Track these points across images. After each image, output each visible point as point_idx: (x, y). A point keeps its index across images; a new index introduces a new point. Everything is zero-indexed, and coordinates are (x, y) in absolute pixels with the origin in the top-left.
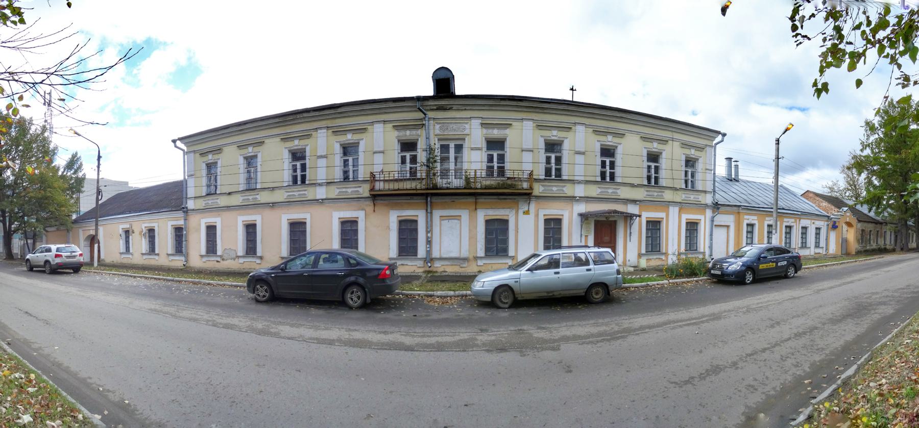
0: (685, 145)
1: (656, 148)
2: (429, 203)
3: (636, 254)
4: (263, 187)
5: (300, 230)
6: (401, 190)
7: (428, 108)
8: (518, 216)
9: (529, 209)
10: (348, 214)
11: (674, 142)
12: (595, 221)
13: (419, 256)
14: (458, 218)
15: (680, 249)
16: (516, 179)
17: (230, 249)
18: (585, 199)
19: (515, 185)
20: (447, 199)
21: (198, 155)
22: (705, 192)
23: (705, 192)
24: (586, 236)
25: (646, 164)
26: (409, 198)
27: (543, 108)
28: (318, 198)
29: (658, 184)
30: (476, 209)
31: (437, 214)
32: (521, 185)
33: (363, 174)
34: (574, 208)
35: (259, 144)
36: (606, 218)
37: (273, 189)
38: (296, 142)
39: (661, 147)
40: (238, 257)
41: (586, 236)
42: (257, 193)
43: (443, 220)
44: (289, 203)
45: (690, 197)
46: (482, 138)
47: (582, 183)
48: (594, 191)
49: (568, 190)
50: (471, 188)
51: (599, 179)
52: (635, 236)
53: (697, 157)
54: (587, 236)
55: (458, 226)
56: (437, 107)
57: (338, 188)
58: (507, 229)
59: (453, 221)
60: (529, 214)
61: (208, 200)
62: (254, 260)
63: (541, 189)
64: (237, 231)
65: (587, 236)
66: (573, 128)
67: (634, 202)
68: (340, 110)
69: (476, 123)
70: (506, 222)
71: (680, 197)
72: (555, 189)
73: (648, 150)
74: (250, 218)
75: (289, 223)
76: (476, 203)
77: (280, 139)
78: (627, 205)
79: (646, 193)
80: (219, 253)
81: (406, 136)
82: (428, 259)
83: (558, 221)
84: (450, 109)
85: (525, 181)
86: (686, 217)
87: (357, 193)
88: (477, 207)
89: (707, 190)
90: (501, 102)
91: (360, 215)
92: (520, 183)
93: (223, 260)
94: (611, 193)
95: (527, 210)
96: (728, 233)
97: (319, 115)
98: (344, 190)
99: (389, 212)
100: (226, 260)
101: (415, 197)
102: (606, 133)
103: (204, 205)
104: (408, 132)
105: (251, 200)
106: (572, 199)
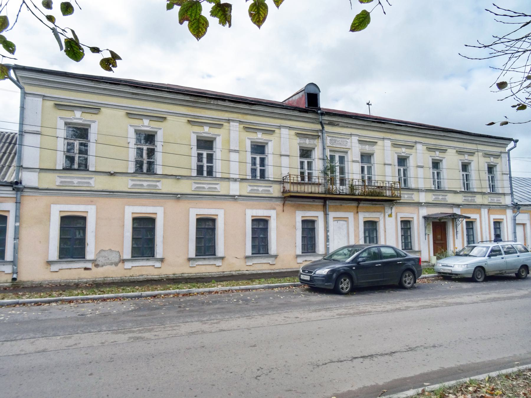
0: (487, 155)
4: (164, 173)
5: (206, 227)
6: (301, 193)
10: (261, 213)
11: (479, 153)
14: (346, 219)
21: (50, 104)
22: (504, 194)
23: (504, 194)
25: (195, 152)
26: (311, 200)
30: (357, 212)
33: (271, 173)
35: (161, 120)
39: (470, 158)
40: (124, 261)
45: (494, 200)
51: (194, 173)
52: (460, 235)
53: (495, 164)
55: (346, 225)
57: (250, 186)
62: (150, 263)
68: (254, 108)
69: (355, 139)
71: (486, 200)
73: (463, 161)
76: (358, 207)
77: (186, 121)
79: (464, 198)
81: (306, 144)
84: (337, 125)
86: (493, 217)
87: (267, 192)
88: (359, 210)
89: (505, 192)
90: (372, 124)
93: (97, 266)
94: (77, 183)
95: (390, 213)
96: (524, 230)
97: (233, 107)
98: (255, 188)
99: (295, 213)
100: (102, 266)
101: (316, 200)
102: (141, 116)
103: (58, 183)
104: (307, 141)
105: (145, 188)
106: (419, 204)
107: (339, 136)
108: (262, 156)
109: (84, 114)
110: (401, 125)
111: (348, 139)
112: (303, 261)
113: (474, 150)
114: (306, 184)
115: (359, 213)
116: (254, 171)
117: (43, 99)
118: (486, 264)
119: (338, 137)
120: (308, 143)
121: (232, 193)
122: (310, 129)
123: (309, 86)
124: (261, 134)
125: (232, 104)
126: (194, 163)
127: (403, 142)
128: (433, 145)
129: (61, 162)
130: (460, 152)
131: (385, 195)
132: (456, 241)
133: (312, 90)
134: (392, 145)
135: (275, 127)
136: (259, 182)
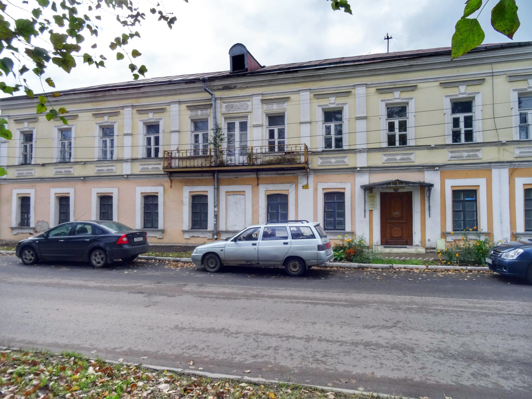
1: (465, 93)
2: (216, 179)
3: (439, 232)
7: (215, 88)
8: (298, 190)
9: (307, 183)
10: (150, 189)
12: (381, 193)
13: (209, 229)
14: (242, 193)
15: (515, 229)
16: (295, 153)
17: (43, 220)
18: (368, 169)
19: (293, 159)
20: (232, 176)
24: (371, 211)
25: (449, 117)
26: (200, 174)
27: (319, 75)
28: (124, 173)
29: (472, 140)
30: (258, 185)
31: (223, 189)
32: (300, 159)
34: (356, 179)
36: (394, 189)
37: (85, 163)
38: (106, 118)
41: (370, 210)
42: (71, 166)
43: (229, 195)
44: (98, 178)
46: (263, 115)
47: (364, 152)
48: (379, 159)
49: (350, 161)
50: (253, 165)
51: (385, 145)
54: (372, 210)
56: (223, 86)
57: (141, 165)
58: (287, 204)
59: (237, 196)
60: (308, 188)
61: (23, 170)
63: (320, 161)
64: (49, 203)
65: (372, 210)
66: (353, 91)
67: (432, 167)
68: (142, 90)
69: (257, 100)
70: (285, 197)
72: (333, 161)
74: (63, 190)
75: (98, 196)
77: (91, 115)
78: (424, 172)
79: (450, 155)
80: (32, 225)
81: (197, 115)
82: (215, 232)
83: (341, 195)
84: (235, 88)
85: (303, 154)
88: (173, 185)
90: (278, 76)
91: (159, 190)
92: (298, 157)
94: (400, 160)
98: (146, 166)
99: (182, 188)
101: (205, 174)
102: (390, 90)
104: (199, 112)
105: (64, 173)
106: (353, 170)
107: (232, 100)
108: (156, 135)
109: (30, 124)
110: (325, 68)
111: (249, 101)
112: (191, 237)
113: (415, 82)
114: (200, 157)
115: (260, 185)
116: (149, 151)
117: (366, 88)
118: (222, 250)
119: (235, 102)
120: (199, 114)
121: (125, 173)
122: (202, 99)
123: (234, 49)
124: (152, 114)
125: (123, 92)
126: (449, 128)
127: (333, 89)
128: (389, 84)
129: (141, 153)
130: (513, 77)
131: (298, 161)
132: (428, 221)
133: (237, 52)
134: (314, 97)
135: (166, 104)
136: (399, 149)
